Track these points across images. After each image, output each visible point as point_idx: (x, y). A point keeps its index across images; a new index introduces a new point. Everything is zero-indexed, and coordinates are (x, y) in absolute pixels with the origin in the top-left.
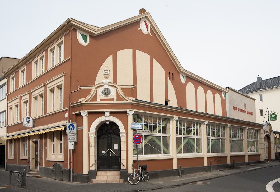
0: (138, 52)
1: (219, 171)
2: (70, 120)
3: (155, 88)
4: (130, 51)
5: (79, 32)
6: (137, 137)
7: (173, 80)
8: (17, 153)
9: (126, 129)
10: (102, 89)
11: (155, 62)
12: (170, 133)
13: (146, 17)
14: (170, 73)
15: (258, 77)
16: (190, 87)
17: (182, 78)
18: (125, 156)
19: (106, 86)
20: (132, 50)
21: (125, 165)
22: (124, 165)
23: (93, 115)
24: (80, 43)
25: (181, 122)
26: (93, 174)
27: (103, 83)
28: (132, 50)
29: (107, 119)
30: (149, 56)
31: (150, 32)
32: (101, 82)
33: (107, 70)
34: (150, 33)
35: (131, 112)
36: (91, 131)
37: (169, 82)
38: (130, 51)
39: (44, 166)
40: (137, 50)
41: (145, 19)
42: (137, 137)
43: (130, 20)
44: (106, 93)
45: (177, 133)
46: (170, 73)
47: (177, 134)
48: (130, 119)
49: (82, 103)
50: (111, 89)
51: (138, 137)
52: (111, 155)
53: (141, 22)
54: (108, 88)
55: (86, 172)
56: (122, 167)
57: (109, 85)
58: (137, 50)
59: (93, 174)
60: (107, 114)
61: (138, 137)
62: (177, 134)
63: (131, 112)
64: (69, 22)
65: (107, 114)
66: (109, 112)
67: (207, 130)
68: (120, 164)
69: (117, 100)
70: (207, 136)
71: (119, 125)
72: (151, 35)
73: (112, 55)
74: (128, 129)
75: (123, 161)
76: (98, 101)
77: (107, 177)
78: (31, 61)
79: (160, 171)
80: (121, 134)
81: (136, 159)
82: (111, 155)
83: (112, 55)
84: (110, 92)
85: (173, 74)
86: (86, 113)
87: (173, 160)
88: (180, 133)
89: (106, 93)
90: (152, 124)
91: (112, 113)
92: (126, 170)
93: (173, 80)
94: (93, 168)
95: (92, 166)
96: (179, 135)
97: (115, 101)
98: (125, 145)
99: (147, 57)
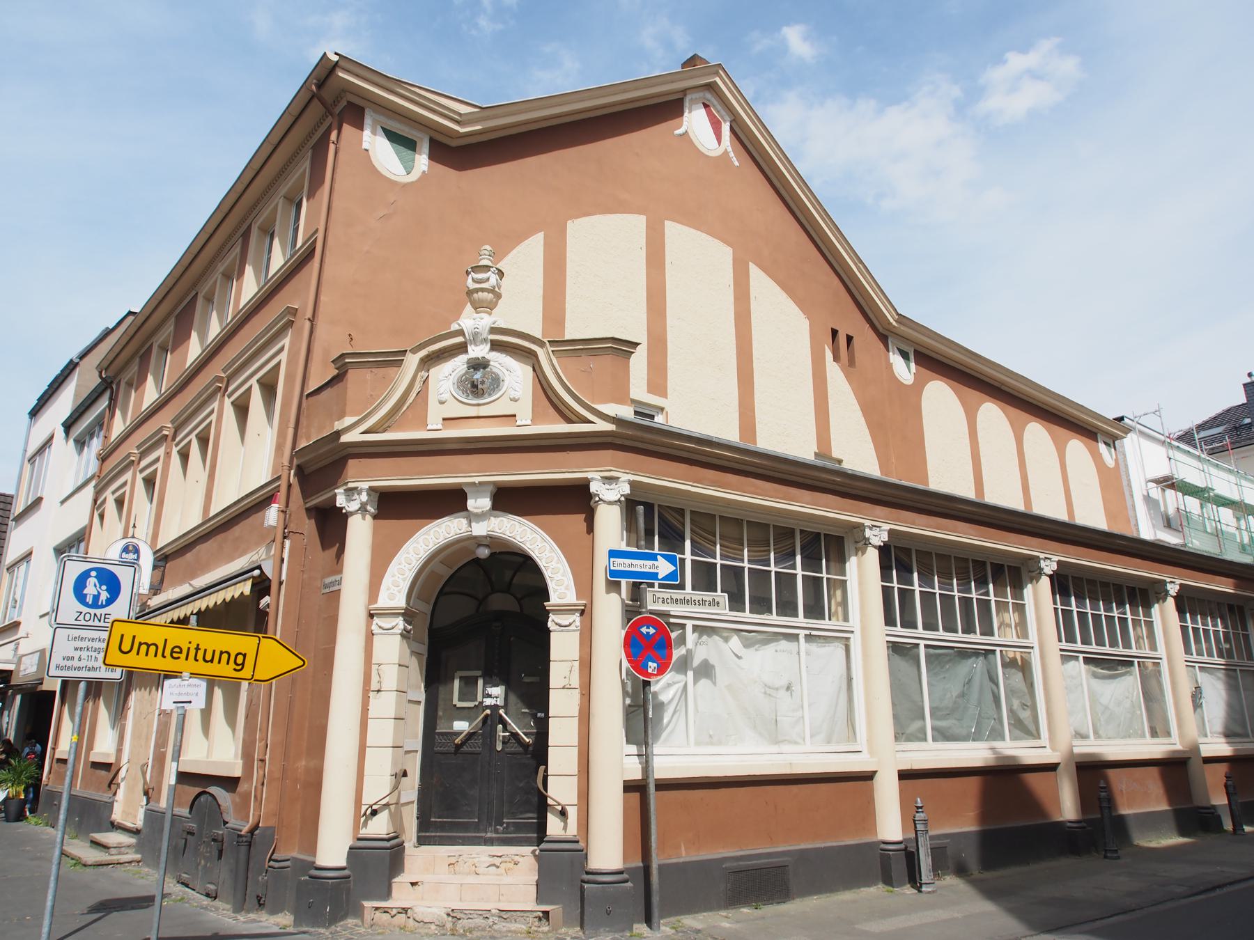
0: (673, 230)
1: (622, 681)
2: (287, 542)
3: (744, 371)
4: (635, 224)
5: (375, 122)
6: (644, 630)
7: (852, 362)
8: (86, 734)
9: (584, 585)
10: (457, 365)
11: (759, 280)
12: (846, 619)
13: (712, 87)
14: (834, 333)
15: (1248, 380)
16: (940, 398)
17: (896, 360)
18: (574, 753)
19: (478, 351)
20: (643, 218)
21: (572, 813)
22: (563, 814)
23: (399, 507)
24: (379, 169)
25: (905, 558)
26: (377, 864)
27: (461, 332)
28: (643, 218)
29: (480, 529)
30: (728, 251)
31: (730, 149)
32: (454, 327)
33: (487, 268)
34: (732, 154)
35: (611, 486)
36: (383, 602)
37: (834, 372)
38: (635, 224)
39: (163, 804)
40: (668, 223)
41: (708, 96)
42: (644, 630)
43: (637, 89)
44: (474, 386)
45: (889, 621)
46: (834, 333)
47: (887, 624)
48: (610, 525)
49: (345, 439)
50: (502, 363)
51: (652, 631)
52: (499, 748)
53: (687, 104)
54: (487, 357)
55: (332, 851)
56: (554, 826)
57: (496, 346)
58: (668, 223)
59: (377, 864)
60: (479, 503)
61: (652, 631)
62: (887, 624)
63: (611, 486)
64: (326, 72)
65: (479, 503)
66: (491, 488)
67: (1056, 609)
68: (541, 806)
69: (534, 421)
70: (1060, 640)
71: (542, 564)
72: (737, 164)
73: (541, 235)
74: (582, 580)
75: (561, 790)
76: (434, 429)
77: (489, 877)
78: (193, 293)
79: (803, 855)
80: (552, 616)
81: (637, 775)
82: (499, 748)
83: (541, 235)
84: (496, 382)
85: (849, 339)
86: (364, 497)
87: (878, 781)
88: (909, 623)
89: (474, 386)
90: (742, 561)
91: (509, 499)
92: (576, 852)
93: (852, 362)
94: (379, 827)
95: (374, 813)
96: (898, 630)
97: (527, 424)
98: (575, 682)
99: (720, 255)
